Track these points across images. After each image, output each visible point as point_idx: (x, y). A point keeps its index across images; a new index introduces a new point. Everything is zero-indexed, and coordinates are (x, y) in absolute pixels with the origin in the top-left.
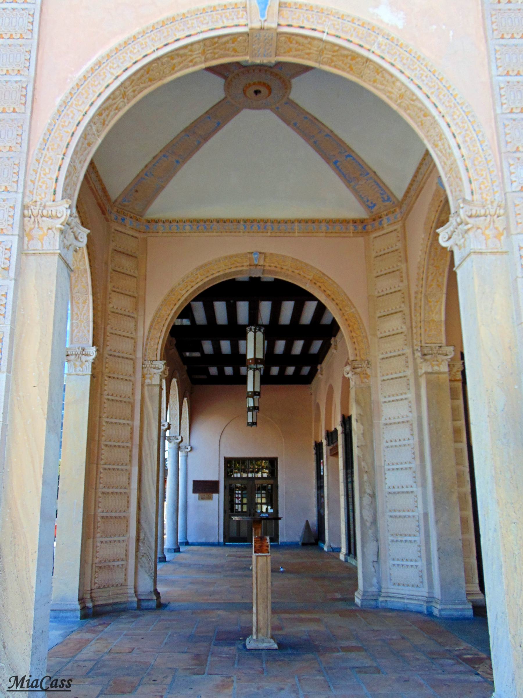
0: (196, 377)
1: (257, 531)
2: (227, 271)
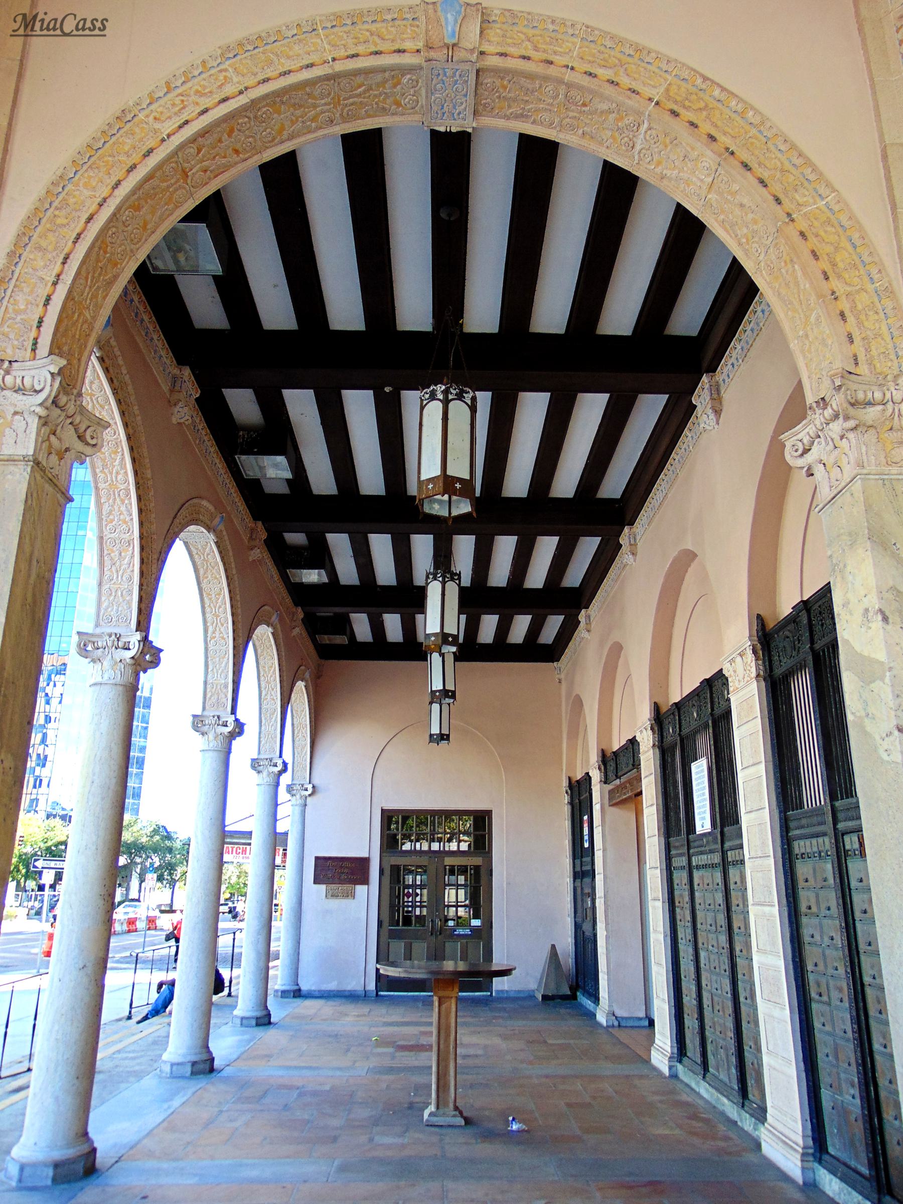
0: (326, 639)
1: (444, 1007)
2: (339, 67)
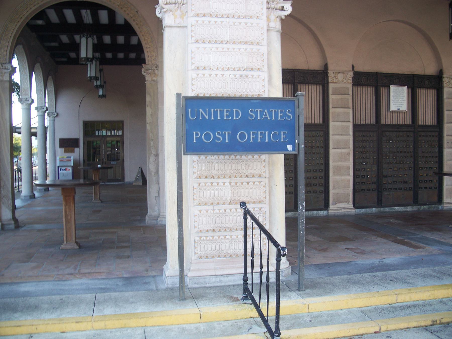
0: (59, 60)
